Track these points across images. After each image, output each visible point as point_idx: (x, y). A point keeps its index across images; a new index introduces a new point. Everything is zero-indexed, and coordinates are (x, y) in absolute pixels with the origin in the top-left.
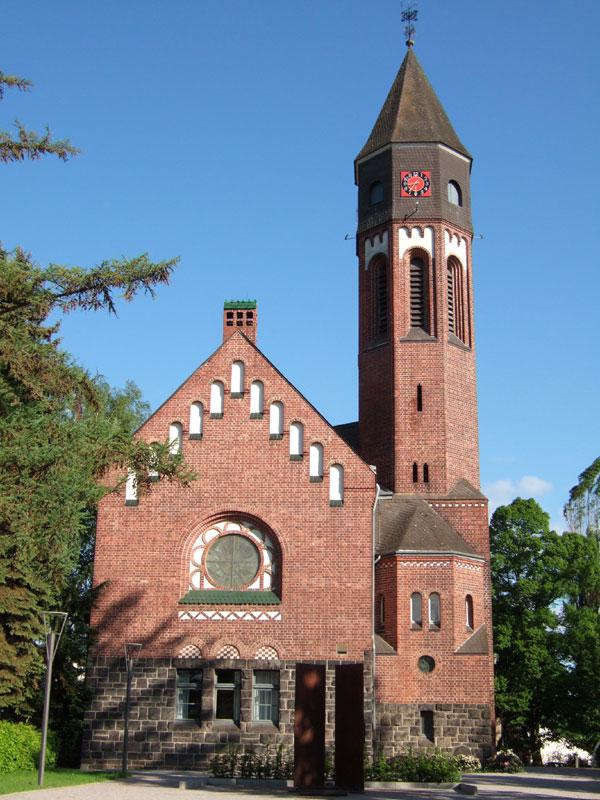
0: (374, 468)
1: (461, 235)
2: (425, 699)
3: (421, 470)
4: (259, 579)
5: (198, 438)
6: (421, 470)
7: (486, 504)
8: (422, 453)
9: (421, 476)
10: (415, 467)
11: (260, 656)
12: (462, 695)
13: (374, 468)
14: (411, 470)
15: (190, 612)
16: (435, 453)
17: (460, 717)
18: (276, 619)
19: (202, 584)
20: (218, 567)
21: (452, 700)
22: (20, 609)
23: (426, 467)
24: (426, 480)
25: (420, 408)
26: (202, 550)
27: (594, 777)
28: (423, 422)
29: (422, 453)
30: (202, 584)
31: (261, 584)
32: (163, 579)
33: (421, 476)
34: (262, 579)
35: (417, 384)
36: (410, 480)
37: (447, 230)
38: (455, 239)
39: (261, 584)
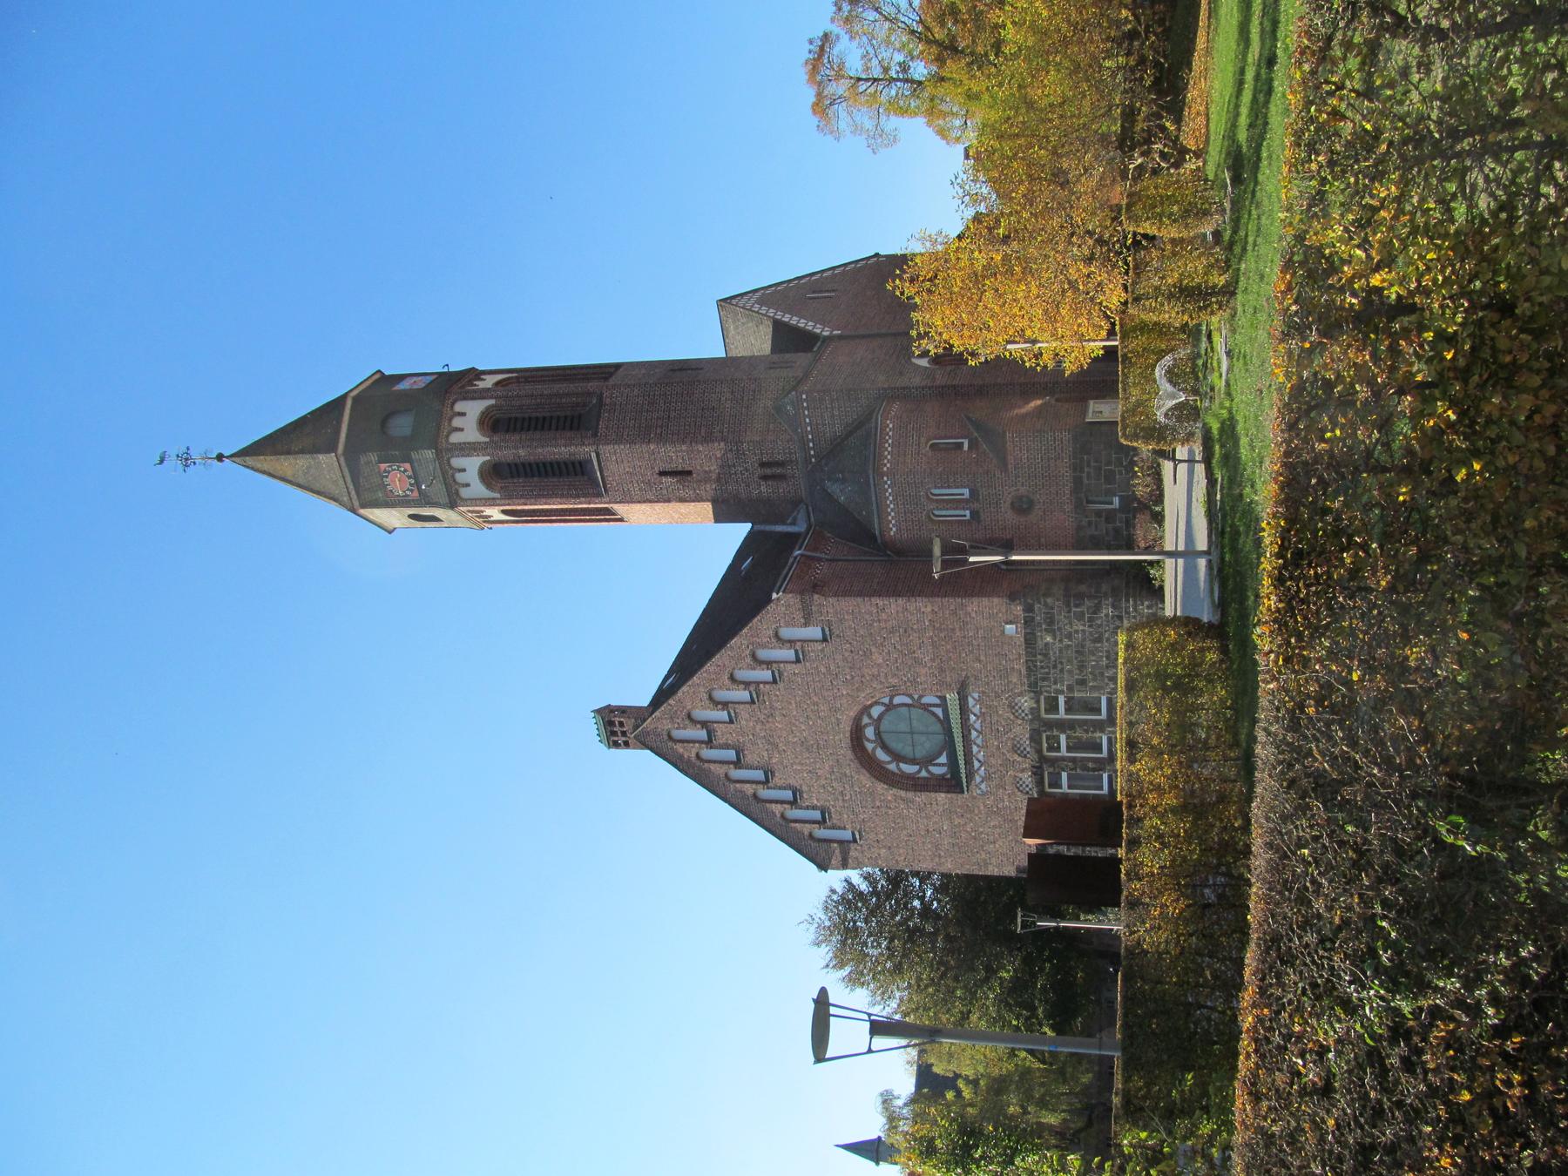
2: (1068, 508)
6: (768, 471)
8: (747, 470)
10: (765, 478)
13: (774, 596)
16: (744, 455)
17: (1089, 466)
19: (943, 765)
23: (763, 465)
25: (689, 473)
34: (931, 705)
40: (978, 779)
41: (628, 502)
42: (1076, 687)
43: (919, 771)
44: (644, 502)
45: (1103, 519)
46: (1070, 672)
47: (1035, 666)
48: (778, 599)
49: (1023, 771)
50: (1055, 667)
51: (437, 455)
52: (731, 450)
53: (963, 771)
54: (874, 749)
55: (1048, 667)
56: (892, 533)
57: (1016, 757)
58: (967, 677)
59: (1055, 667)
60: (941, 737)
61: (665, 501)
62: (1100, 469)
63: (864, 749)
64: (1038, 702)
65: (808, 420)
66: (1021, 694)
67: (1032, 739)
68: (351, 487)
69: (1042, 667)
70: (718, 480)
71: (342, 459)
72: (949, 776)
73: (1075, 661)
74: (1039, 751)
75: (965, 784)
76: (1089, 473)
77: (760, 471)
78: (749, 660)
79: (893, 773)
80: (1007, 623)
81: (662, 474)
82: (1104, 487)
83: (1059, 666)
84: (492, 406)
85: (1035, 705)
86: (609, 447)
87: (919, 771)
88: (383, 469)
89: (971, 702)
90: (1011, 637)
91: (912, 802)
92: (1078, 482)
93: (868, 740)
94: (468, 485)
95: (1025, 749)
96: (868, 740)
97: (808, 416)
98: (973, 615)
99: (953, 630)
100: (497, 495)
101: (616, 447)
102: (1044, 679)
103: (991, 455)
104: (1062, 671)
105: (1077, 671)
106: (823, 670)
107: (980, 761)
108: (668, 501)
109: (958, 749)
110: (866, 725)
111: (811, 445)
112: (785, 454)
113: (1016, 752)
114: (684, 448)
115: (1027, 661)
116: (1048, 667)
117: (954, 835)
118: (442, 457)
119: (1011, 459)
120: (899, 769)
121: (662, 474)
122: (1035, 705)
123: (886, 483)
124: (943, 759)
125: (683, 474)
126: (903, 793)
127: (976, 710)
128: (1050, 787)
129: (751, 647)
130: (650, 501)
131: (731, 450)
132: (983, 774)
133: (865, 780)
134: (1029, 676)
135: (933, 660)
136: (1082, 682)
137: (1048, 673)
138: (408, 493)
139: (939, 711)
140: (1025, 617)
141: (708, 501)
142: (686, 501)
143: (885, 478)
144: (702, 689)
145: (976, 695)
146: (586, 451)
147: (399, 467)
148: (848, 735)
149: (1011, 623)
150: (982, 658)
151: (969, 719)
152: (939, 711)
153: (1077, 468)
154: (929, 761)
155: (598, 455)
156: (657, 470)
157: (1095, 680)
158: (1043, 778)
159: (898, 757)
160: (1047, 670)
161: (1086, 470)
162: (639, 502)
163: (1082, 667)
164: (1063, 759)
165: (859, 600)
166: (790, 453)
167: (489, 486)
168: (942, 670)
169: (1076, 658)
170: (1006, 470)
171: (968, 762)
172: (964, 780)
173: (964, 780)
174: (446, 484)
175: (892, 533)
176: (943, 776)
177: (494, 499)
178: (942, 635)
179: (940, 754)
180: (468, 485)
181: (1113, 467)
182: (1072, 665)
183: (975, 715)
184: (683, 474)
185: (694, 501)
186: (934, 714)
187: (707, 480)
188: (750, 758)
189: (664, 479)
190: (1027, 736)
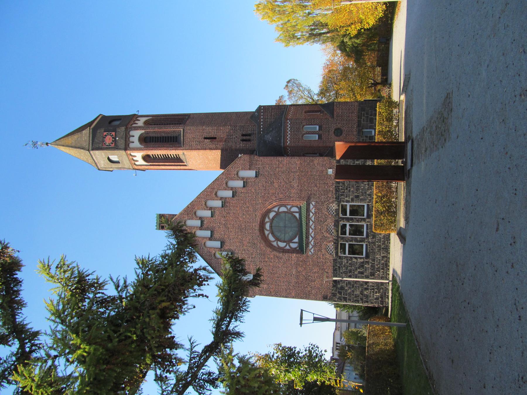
0: (240, 155)
1: (135, 119)
2: (355, 133)
3: (244, 138)
4: (294, 214)
5: (222, 243)
6: (244, 138)
7: (262, 106)
8: (237, 137)
9: (248, 138)
10: (243, 140)
11: (332, 226)
12: (353, 115)
13: (240, 155)
14: (244, 142)
15: (310, 248)
16: (237, 131)
17: (364, 116)
18: (314, 204)
19: (296, 243)
20: (287, 235)
21: (356, 119)
22: (425, 151)
23: (243, 135)
24: (249, 135)
25: (215, 138)
26: (279, 242)
27: (364, 167)
28: (222, 136)
29: (237, 137)
30: (296, 243)
31: (296, 212)
32: (293, 262)
33: (248, 138)
34: (294, 212)
35: (203, 139)
36: (249, 143)
37: (132, 125)
38: (136, 122)
39: (296, 212)
40: (310, 246)
41: (190, 150)
42: (355, 199)
43: (286, 246)
44: (196, 149)
45: (368, 138)
46: (353, 192)
47: (339, 189)
48: (241, 157)
49: (330, 242)
50: (347, 189)
51: (126, 129)
52: (232, 129)
53: (304, 242)
54: (268, 234)
55: (344, 189)
56: (288, 144)
57: (328, 235)
58: (311, 194)
59: (347, 189)
60: (296, 229)
61: (204, 149)
62: (368, 117)
63: (264, 234)
64: (339, 206)
65: (262, 117)
66: (332, 203)
67: (335, 225)
68: (91, 142)
69: (342, 189)
70: (225, 141)
71: (91, 130)
72: (298, 249)
73: (355, 187)
74: (337, 253)
75: (305, 250)
76: (364, 119)
77: (242, 138)
78: (224, 185)
79: (275, 246)
80: (329, 169)
81: (205, 138)
82: (369, 125)
83: (349, 189)
84: (151, 119)
85: (337, 208)
86: (188, 128)
87: (286, 246)
88: (104, 135)
89: (311, 206)
90: (330, 175)
91: (281, 258)
92: (359, 122)
93: (266, 230)
94: (133, 142)
95: (332, 231)
96: (266, 230)
97: (263, 115)
98: (316, 165)
99: (308, 172)
100: (143, 147)
101: (191, 127)
102: (342, 195)
103: (328, 114)
104: (349, 191)
105: (356, 191)
106: (253, 191)
107: (312, 237)
108: (205, 149)
109: (304, 233)
110: (267, 222)
111: (262, 126)
112: (252, 130)
113: (328, 232)
114: (215, 128)
115: (336, 186)
116: (344, 189)
117: (297, 277)
118: (127, 130)
119: (335, 113)
120: (277, 244)
121: (205, 138)
122: (337, 208)
123: (288, 123)
124: (296, 240)
125: (213, 138)
126: (278, 254)
127: (313, 211)
128: (341, 235)
129: (226, 180)
130: (199, 149)
131: (232, 129)
132: (313, 244)
133: (262, 245)
134: (336, 193)
135: (298, 186)
136: (357, 197)
137: (344, 192)
138: (111, 144)
139: (297, 215)
140: (337, 165)
141: (220, 149)
142: (212, 149)
143: (288, 121)
144: (203, 200)
145: (313, 203)
146: (179, 152)
147: (111, 134)
148: (259, 223)
149: (331, 168)
150: (318, 185)
151: (310, 215)
152: (297, 215)
153: (359, 117)
154: (290, 241)
155: (184, 130)
156: (203, 136)
157: (362, 195)
158: (338, 246)
159: (277, 239)
160: (343, 191)
161: (363, 118)
162: (195, 150)
163: (357, 190)
164: (347, 242)
165: (272, 158)
166: (254, 130)
167: (141, 143)
168: (301, 190)
169: (356, 185)
170: (333, 117)
171: (307, 238)
172: (305, 246)
173: (305, 246)
174: (125, 140)
175: (288, 144)
176: (296, 248)
177: (141, 148)
178: (303, 174)
179: (295, 237)
180: (133, 142)
181: (373, 117)
182: (354, 188)
183: (312, 213)
184: (213, 138)
185: (215, 149)
186: (295, 216)
187: (221, 141)
188: (216, 235)
189: (206, 140)
190: (333, 224)
